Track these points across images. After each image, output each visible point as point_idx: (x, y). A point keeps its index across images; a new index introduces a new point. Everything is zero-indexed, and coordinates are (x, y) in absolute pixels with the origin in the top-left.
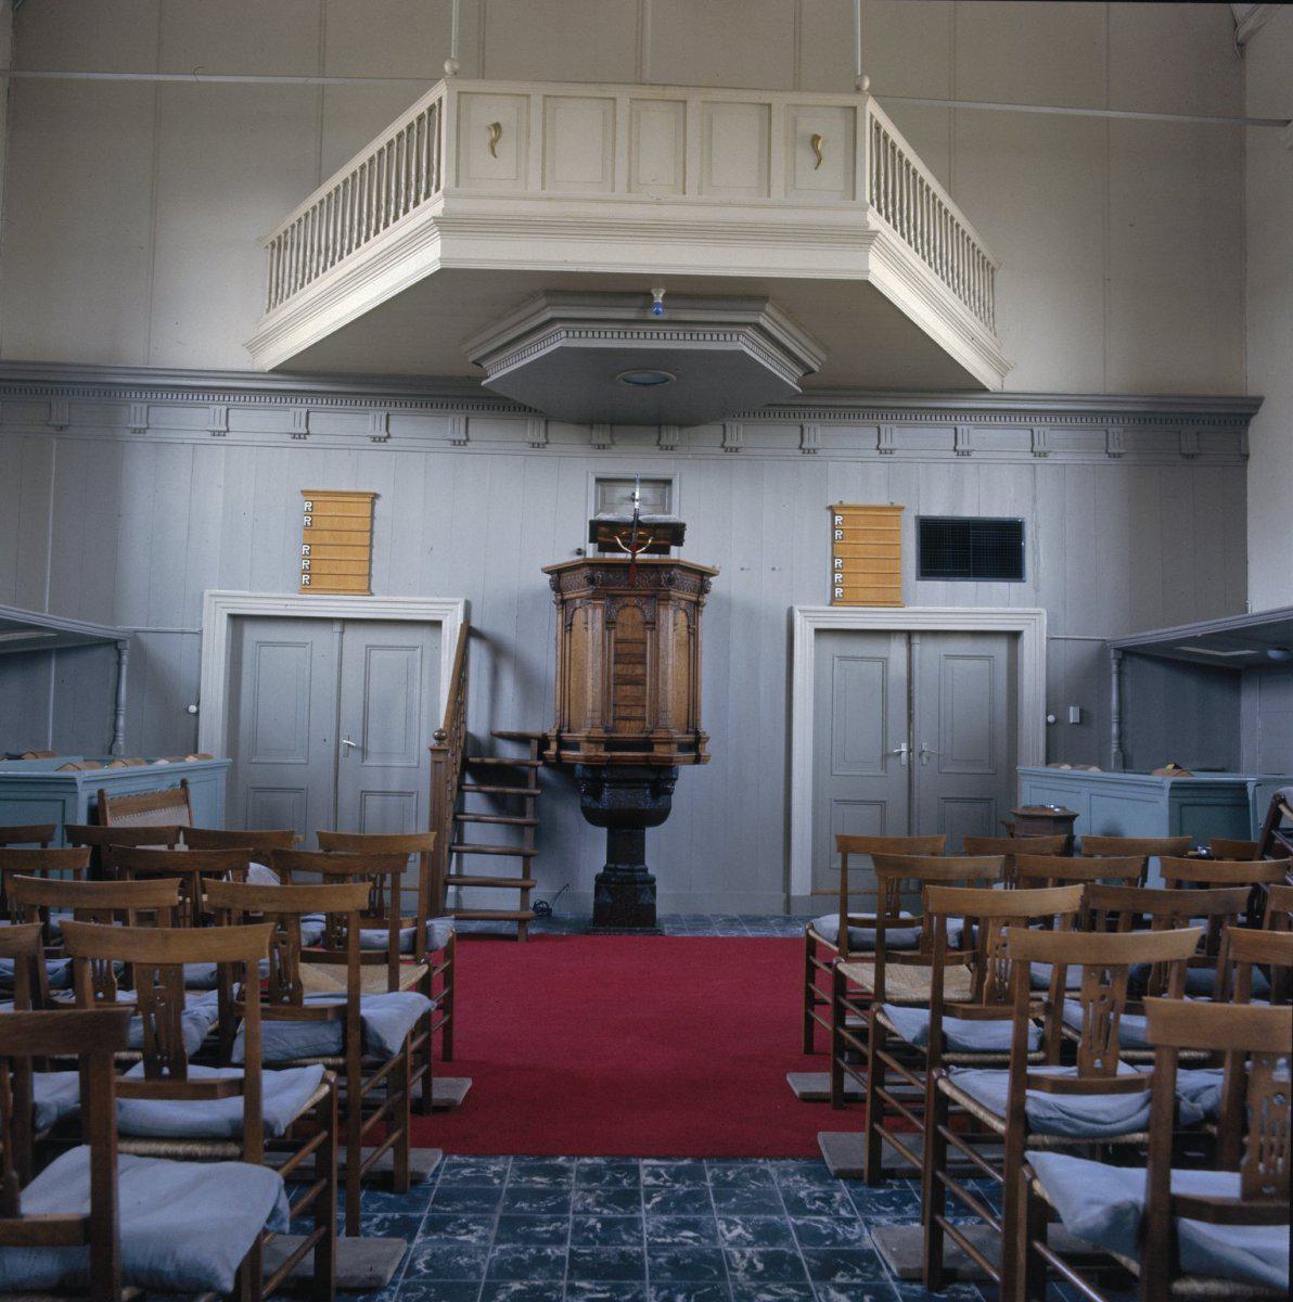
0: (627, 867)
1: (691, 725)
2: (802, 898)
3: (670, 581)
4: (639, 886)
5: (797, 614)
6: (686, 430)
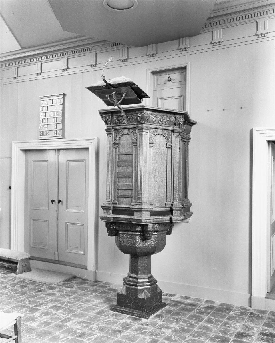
0: (135, 276)
3: (143, 119)
5: (255, 133)
6: (193, 38)
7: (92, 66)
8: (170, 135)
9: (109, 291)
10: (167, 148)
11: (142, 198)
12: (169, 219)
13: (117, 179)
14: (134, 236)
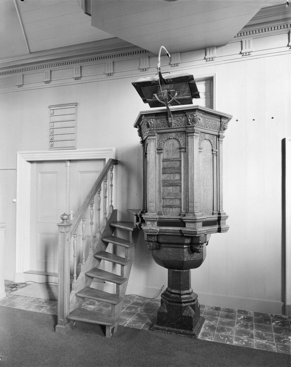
0: (177, 292)
1: (215, 209)
2: (288, 306)
4: (184, 305)
7: (76, 79)
8: (215, 140)
9: (136, 306)
10: (213, 154)
11: (194, 208)
12: (217, 229)
13: (162, 187)
14: (181, 249)
